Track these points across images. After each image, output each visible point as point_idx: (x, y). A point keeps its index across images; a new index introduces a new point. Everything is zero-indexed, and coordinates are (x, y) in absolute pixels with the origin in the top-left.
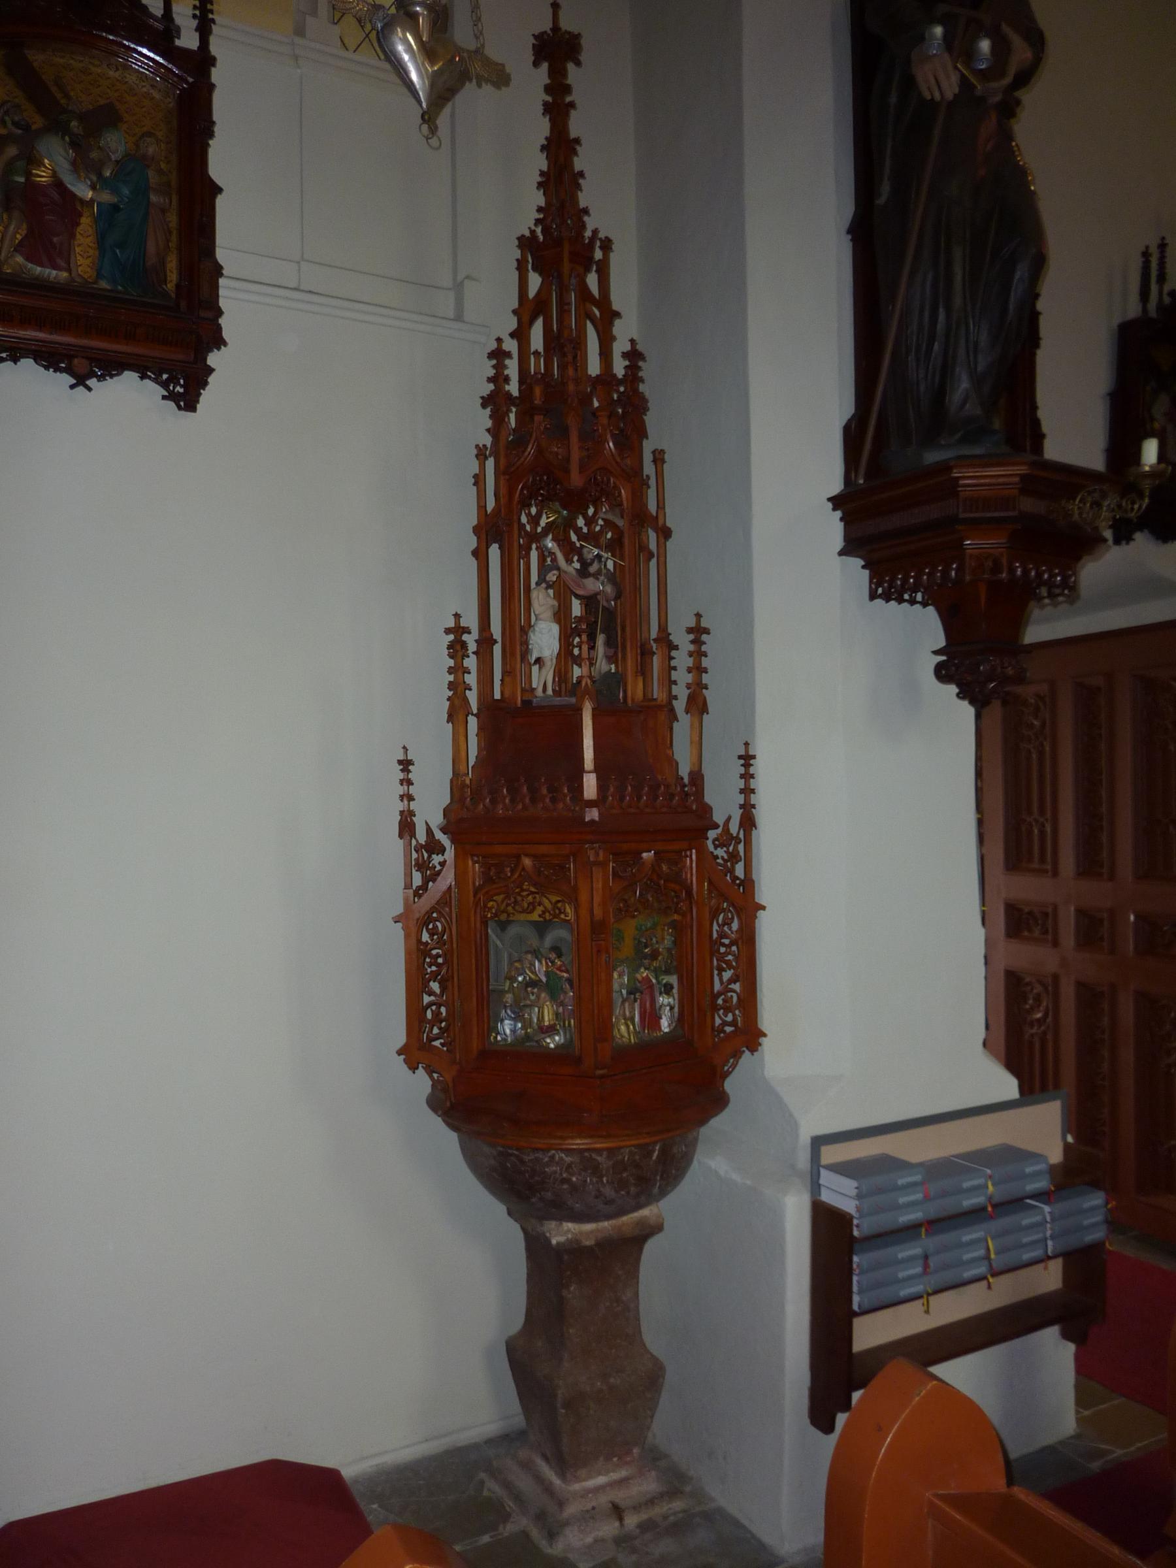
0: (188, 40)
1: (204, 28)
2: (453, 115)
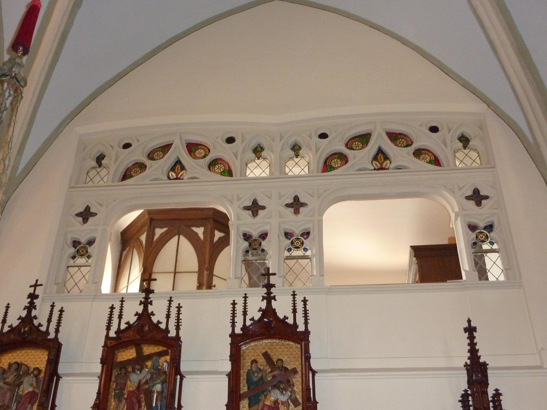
0: (172, 333)
1: (306, 323)
2: (108, 328)
